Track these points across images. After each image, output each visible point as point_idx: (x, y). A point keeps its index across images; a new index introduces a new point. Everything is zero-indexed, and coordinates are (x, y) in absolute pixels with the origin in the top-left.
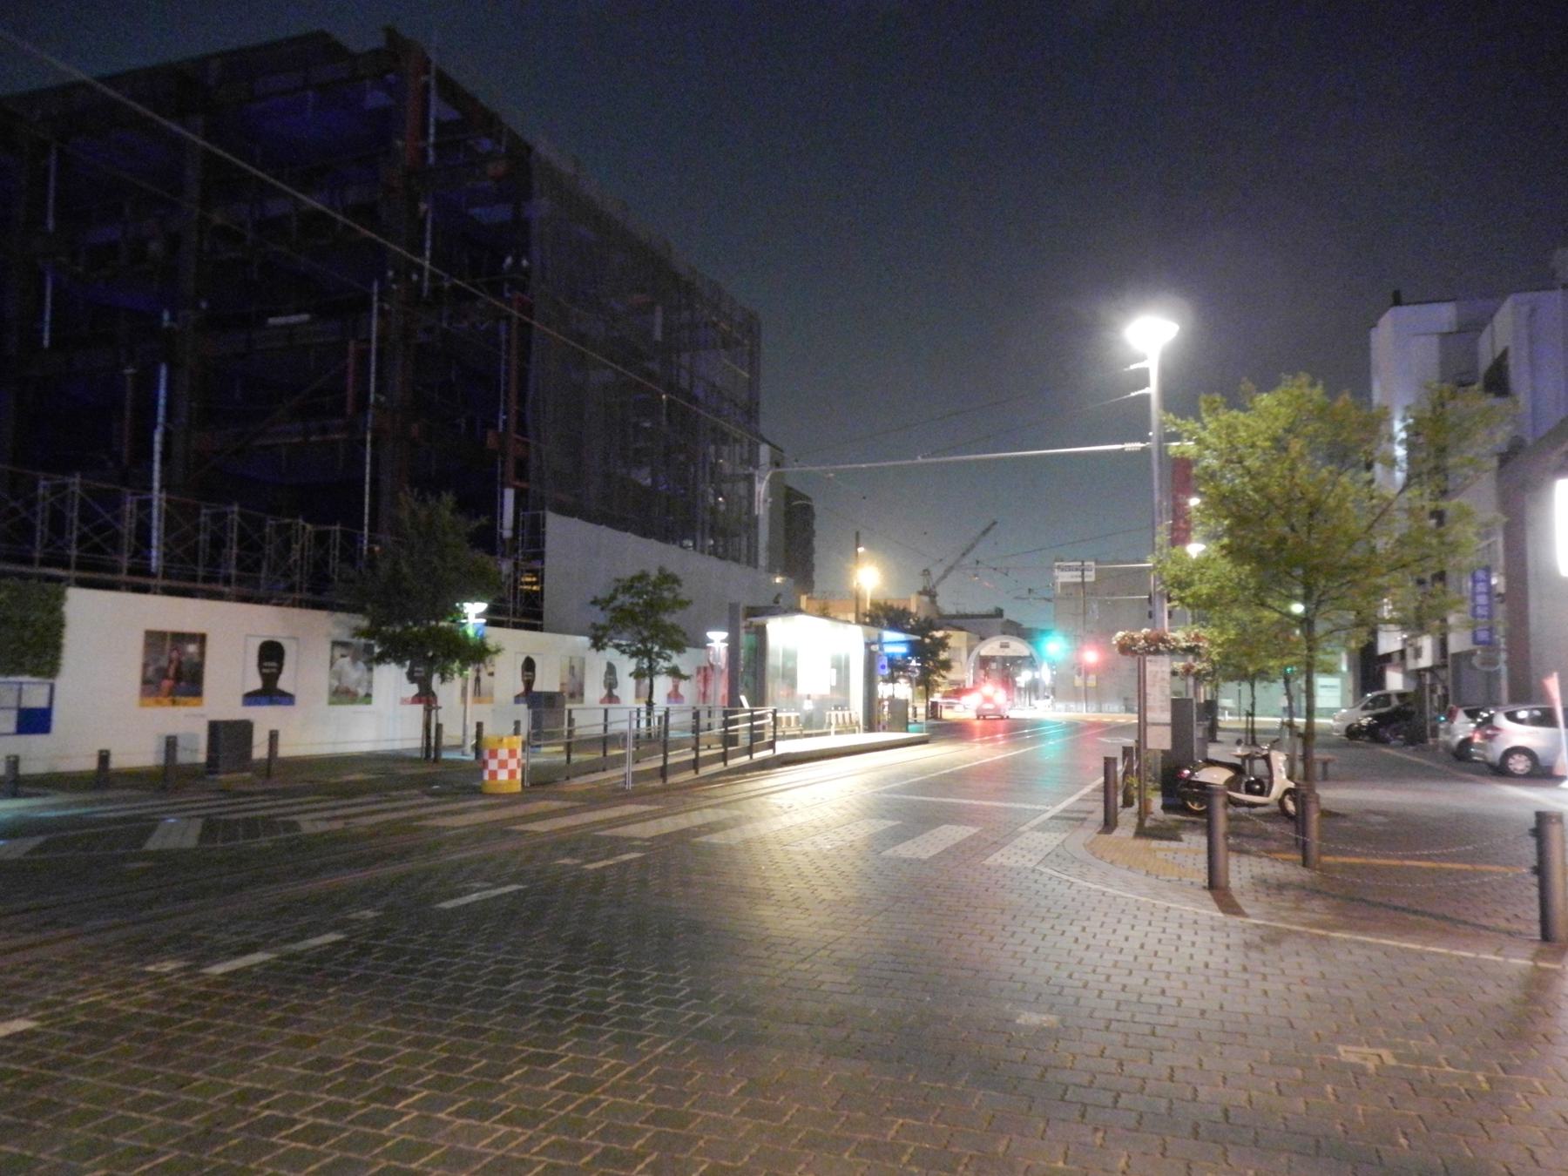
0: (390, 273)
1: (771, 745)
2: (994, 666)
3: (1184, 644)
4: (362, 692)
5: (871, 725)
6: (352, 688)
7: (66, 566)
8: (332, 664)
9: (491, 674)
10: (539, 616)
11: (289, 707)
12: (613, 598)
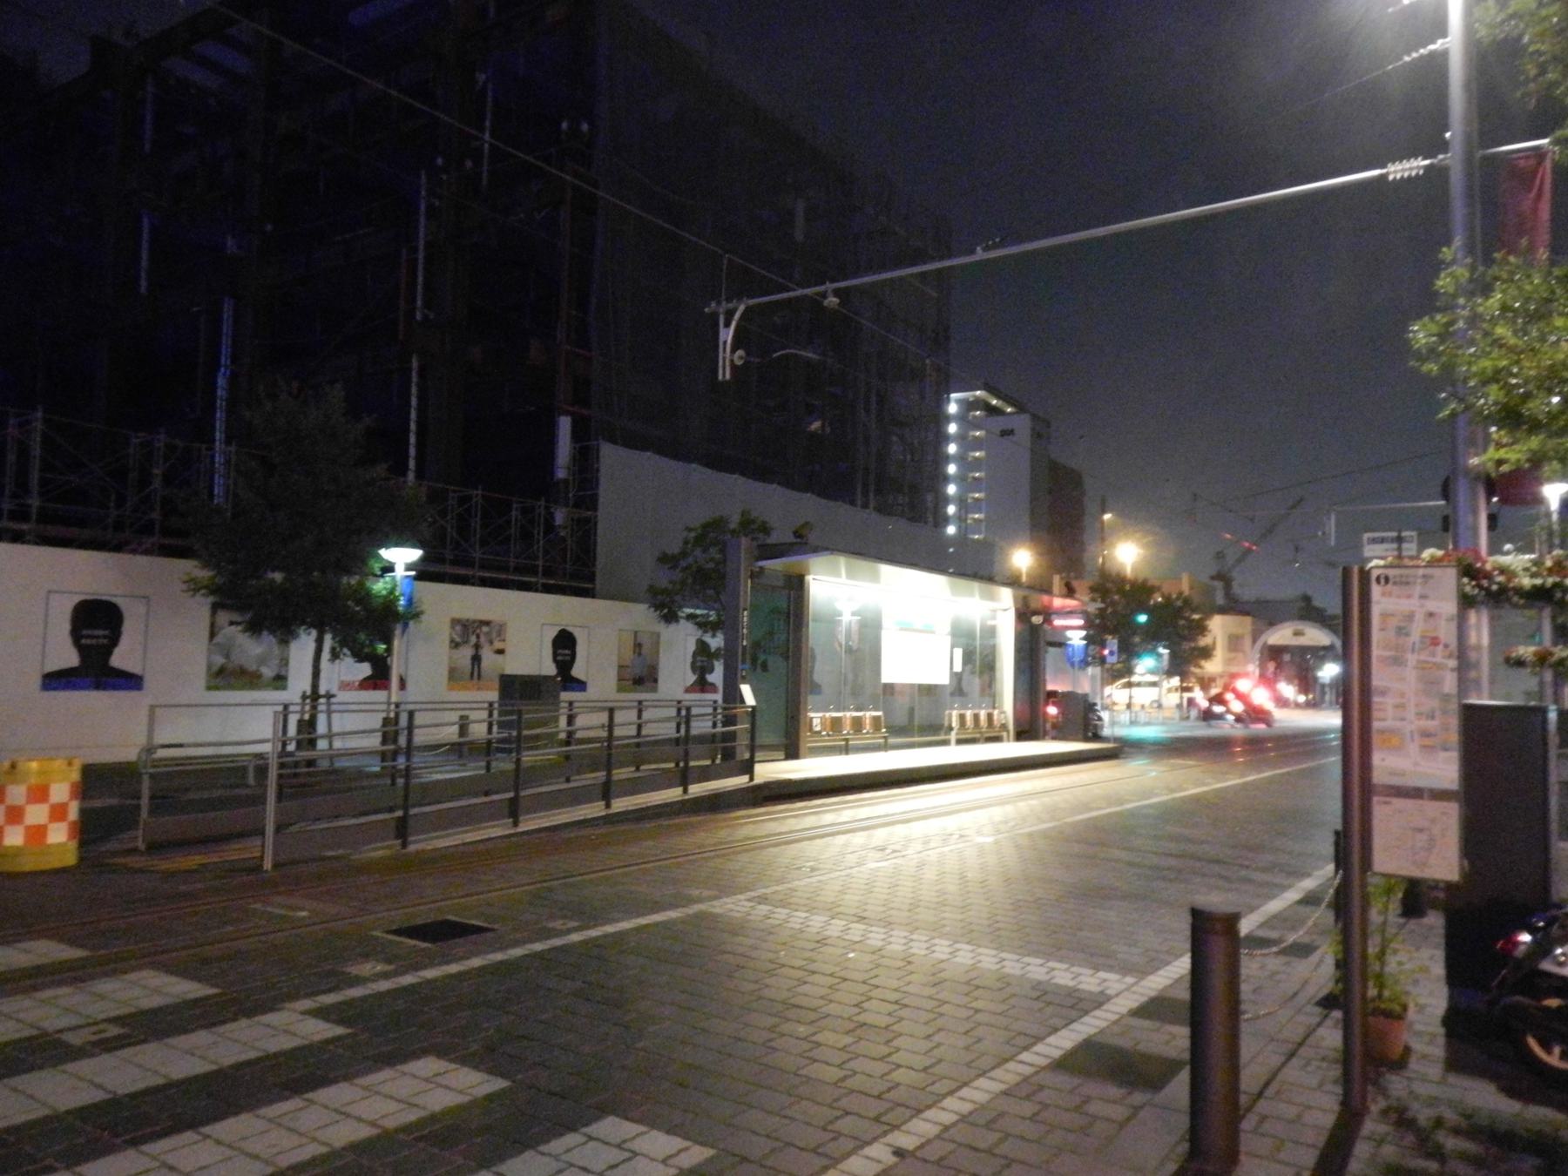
0: (440, 161)
1: (748, 768)
2: (1287, 657)
3: (1527, 582)
4: (268, 672)
5: (1025, 732)
6: (252, 666)
7: (535, 573)
8: (212, 635)
9: (501, 652)
10: (591, 578)
11: (134, 694)
12: (684, 554)
